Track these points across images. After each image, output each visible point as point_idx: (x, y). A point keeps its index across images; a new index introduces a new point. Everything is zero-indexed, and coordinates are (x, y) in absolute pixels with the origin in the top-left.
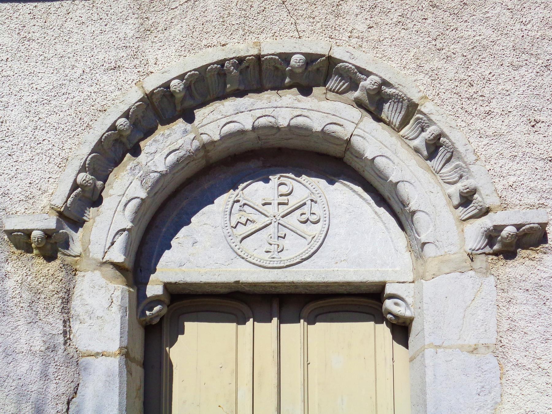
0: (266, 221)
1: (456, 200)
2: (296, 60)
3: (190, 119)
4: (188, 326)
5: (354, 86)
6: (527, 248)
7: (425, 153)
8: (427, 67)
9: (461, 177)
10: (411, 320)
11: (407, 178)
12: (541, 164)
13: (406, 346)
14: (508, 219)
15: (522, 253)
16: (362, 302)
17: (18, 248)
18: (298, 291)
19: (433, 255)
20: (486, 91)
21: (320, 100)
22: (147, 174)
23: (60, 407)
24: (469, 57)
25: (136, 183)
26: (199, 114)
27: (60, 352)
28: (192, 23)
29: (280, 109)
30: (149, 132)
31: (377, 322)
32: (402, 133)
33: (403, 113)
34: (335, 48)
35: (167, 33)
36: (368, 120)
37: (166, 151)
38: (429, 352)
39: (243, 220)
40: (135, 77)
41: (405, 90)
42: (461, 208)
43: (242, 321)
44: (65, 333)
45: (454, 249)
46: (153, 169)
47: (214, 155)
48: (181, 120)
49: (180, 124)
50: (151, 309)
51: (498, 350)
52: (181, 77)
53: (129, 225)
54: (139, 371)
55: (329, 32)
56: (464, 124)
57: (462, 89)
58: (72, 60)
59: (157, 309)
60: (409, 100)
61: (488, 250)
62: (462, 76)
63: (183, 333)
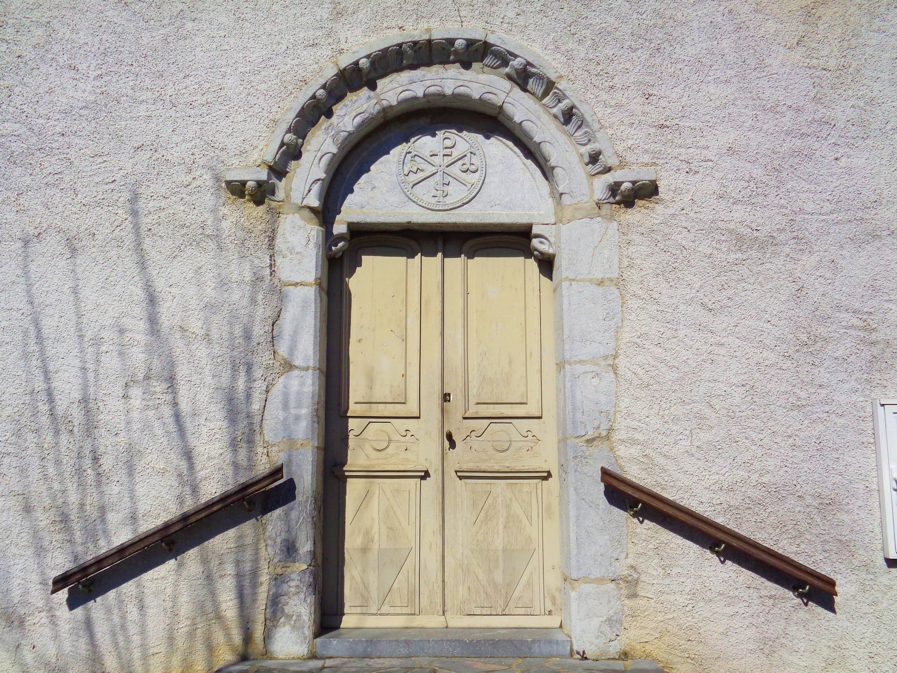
0: (434, 170)
1: (587, 160)
2: (460, 44)
3: (373, 87)
4: (365, 259)
5: (505, 63)
6: (642, 199)
7: (562, 120)
8: (563, 49)
9: (590, 141)
10: (554, 256)
11: (548, 139)
12: (653, 130)
13: (551, 278)
14: (626, 177)
15: (639, 202)
16: (513, 240)
17: (233, 194)
18: (459, 229)
19: (568, 203)
20: (610, 69)
21: (478, 73)
22: (338, 133)
23: (267, 328)
24: (597, 40)
25: (329, 140)
26: (381, 83)
27: (267, 282)
28: (375, 9)
29: (446, 80)
30: (340, 98)
31: (526, 257)
32: (544, 101)
33: (544, 87)
34: (490, 35)
35: (355, 16)
36: (517, 90)
37: (354, 114)
38: (565, 284)
39: (415, 169)
40: (329, 53)
41: (544, 71)
42: (590, 166)
43: (411, 255)
44: (271, 265)
45: (586, 199)
46: (343, 129)
47: (390, 114)
48: (366, 88)
49: (365, 92)
50: (336, 245)
51: (619, 282)
52: (368, 57)
53: (323, 176)
54: (325, 298)
55: (485, 18)
56: (592, 96)
57: (592, 67)
58: (278, 37)
59: (341, 244)
60: (548, 78)
61: (612, 200)
62: (591, 56)
63: (360, 266)
